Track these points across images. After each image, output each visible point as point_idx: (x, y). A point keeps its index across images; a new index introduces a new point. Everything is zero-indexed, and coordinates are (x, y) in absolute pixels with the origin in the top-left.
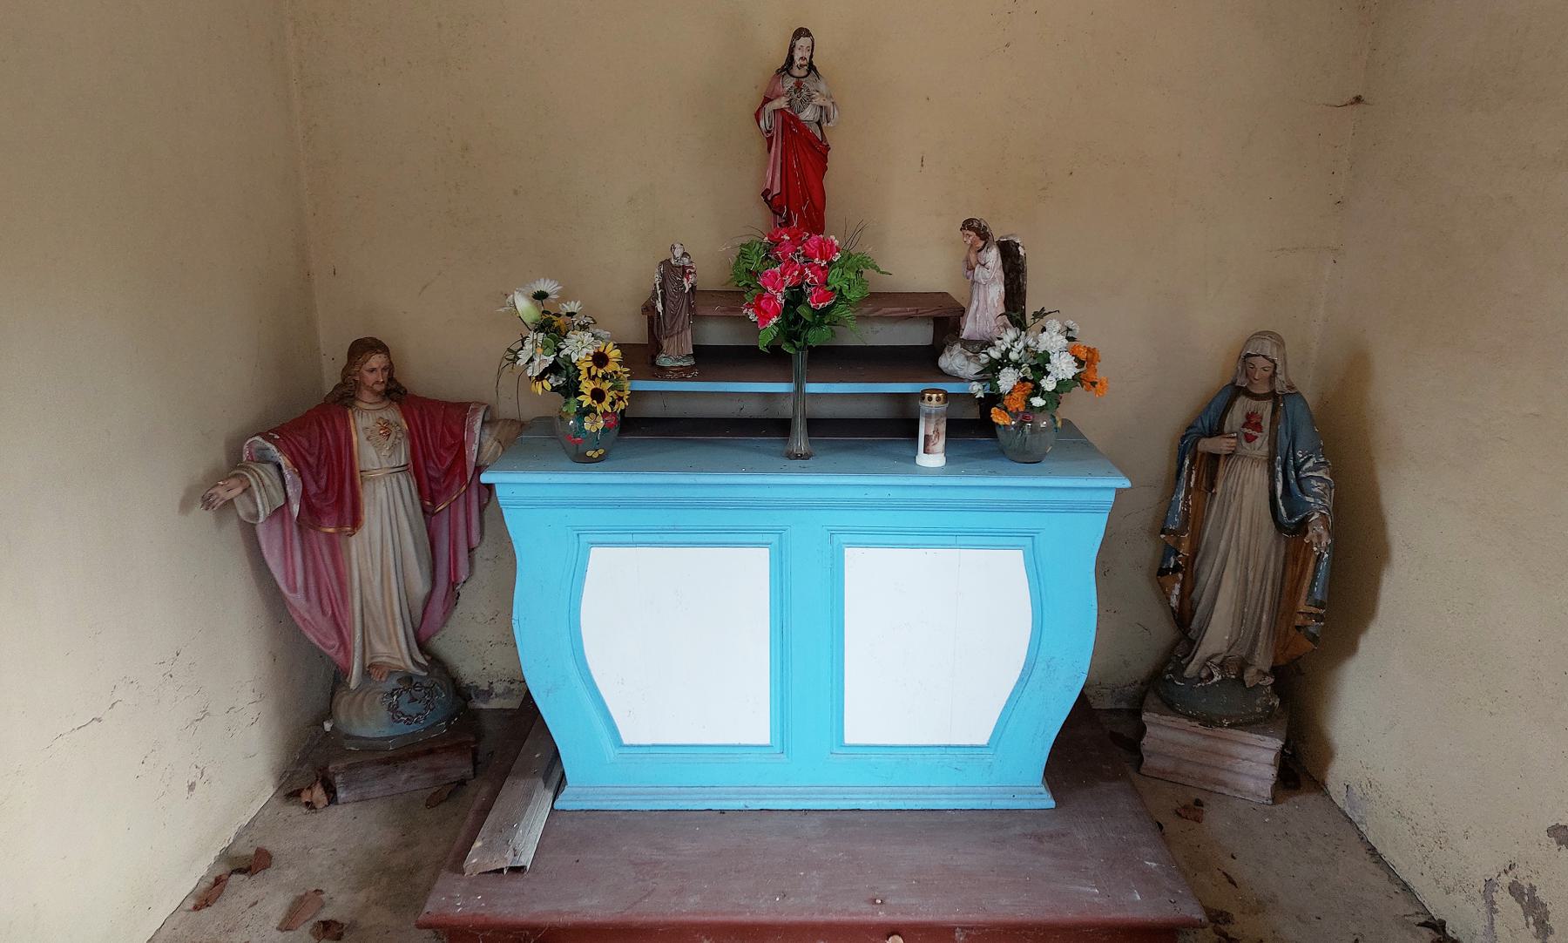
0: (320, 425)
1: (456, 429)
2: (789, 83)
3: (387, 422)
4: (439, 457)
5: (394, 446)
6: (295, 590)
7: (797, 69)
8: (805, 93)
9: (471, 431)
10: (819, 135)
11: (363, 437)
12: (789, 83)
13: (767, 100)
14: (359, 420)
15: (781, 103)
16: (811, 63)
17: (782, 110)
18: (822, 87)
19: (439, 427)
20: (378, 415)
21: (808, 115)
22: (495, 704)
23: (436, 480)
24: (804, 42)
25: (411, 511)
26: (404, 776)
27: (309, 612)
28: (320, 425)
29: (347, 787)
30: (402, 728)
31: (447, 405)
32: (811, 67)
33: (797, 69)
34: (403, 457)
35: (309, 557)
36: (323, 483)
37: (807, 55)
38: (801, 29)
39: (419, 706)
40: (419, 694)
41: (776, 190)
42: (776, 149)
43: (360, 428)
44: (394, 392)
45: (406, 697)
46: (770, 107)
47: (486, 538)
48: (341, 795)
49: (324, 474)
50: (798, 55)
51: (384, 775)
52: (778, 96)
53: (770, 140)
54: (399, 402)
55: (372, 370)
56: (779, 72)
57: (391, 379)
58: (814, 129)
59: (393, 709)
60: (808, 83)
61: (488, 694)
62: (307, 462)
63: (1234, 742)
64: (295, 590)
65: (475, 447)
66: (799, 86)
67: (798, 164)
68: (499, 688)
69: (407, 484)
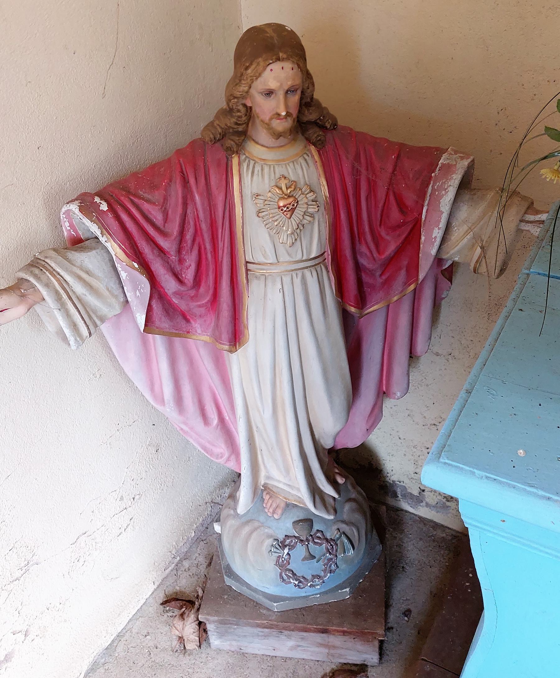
0: (185, 182)
1: (410, 198)
3: (293, 185)
4: (378, 241)
5: (301, 226)
6: (162, 402)
9: (436, 200)
11: (251, 208)
14: (247, 179)
19: (381, 193)
20: (280, 171)
22: (423, 512)
23: (371, 273)
25: (320, 326)
26: (291, 643)
27: (185, 423)
28: (185, 182)
29: (221, 635)
30: (290, 590)
31: (402, 151)
34: (316, 241)
35: (183, 368)
36: (189, 275)
39: (316, 567)
40: (317, 550)
43: (247, 192)
44: (310, 123)
45: (300, 551)
47: (441, 327)
48: (215, 640)
49: (191, 261)
51: (266, 636)
54: (320, 145)
55: (269, 93)
57: (307, 102)
59: (283, 566)
61: (418, 499)
62: (161, 250)
64: (162, 402)
65: (437, 233)
68: (430, 498)
69: (318, 290)
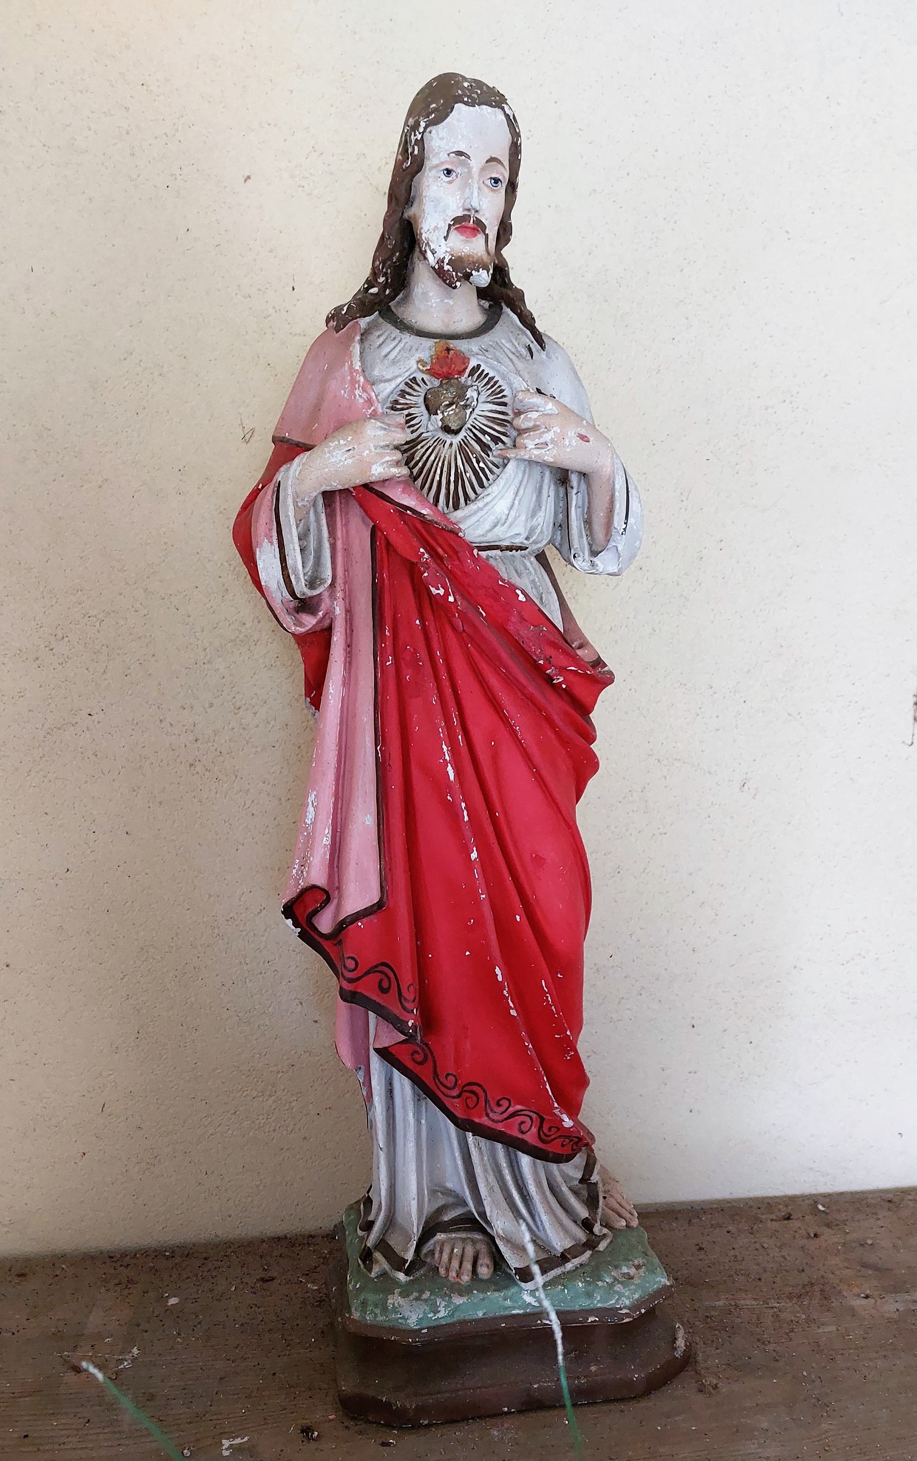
2: (398, 360)
7: (424, 277)
8: (482, 408)
10: (557, 620)
12: (398, 360)
13: (287, 450)
15: (366, 453)
16: (500, 272)
17: (368, 494)
18: (558, 383)
21: (500, 514)
24: (466, 131)
32: (500, 296)
33: (424, 277)
37: (489, 208)
38: (383, 992)
41: (360, 891)
42: (351, 682)
46: (305, 478)
50: (438, 206)
52: (343, 423)
53: (315, 649)
56: (339, 319)
58: (527, 580)
60: (496, 354)
63: (391, 1222)
66: (448, 368)
67: (462, 681)
